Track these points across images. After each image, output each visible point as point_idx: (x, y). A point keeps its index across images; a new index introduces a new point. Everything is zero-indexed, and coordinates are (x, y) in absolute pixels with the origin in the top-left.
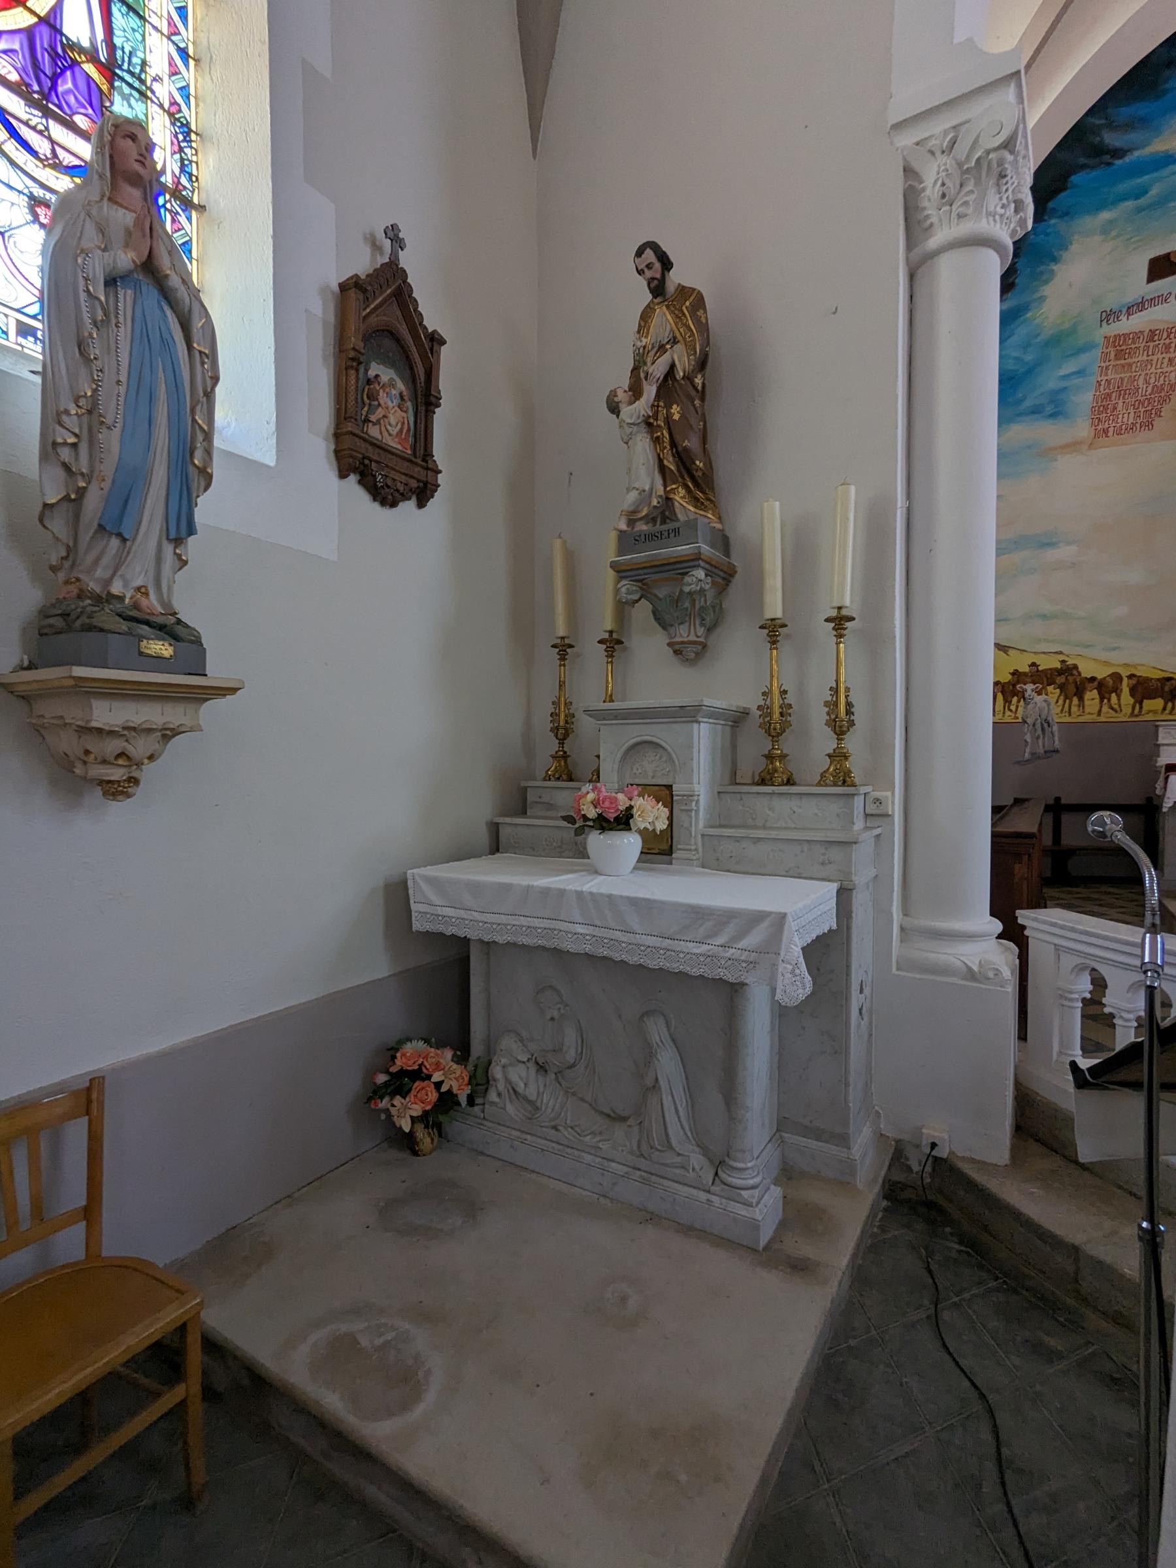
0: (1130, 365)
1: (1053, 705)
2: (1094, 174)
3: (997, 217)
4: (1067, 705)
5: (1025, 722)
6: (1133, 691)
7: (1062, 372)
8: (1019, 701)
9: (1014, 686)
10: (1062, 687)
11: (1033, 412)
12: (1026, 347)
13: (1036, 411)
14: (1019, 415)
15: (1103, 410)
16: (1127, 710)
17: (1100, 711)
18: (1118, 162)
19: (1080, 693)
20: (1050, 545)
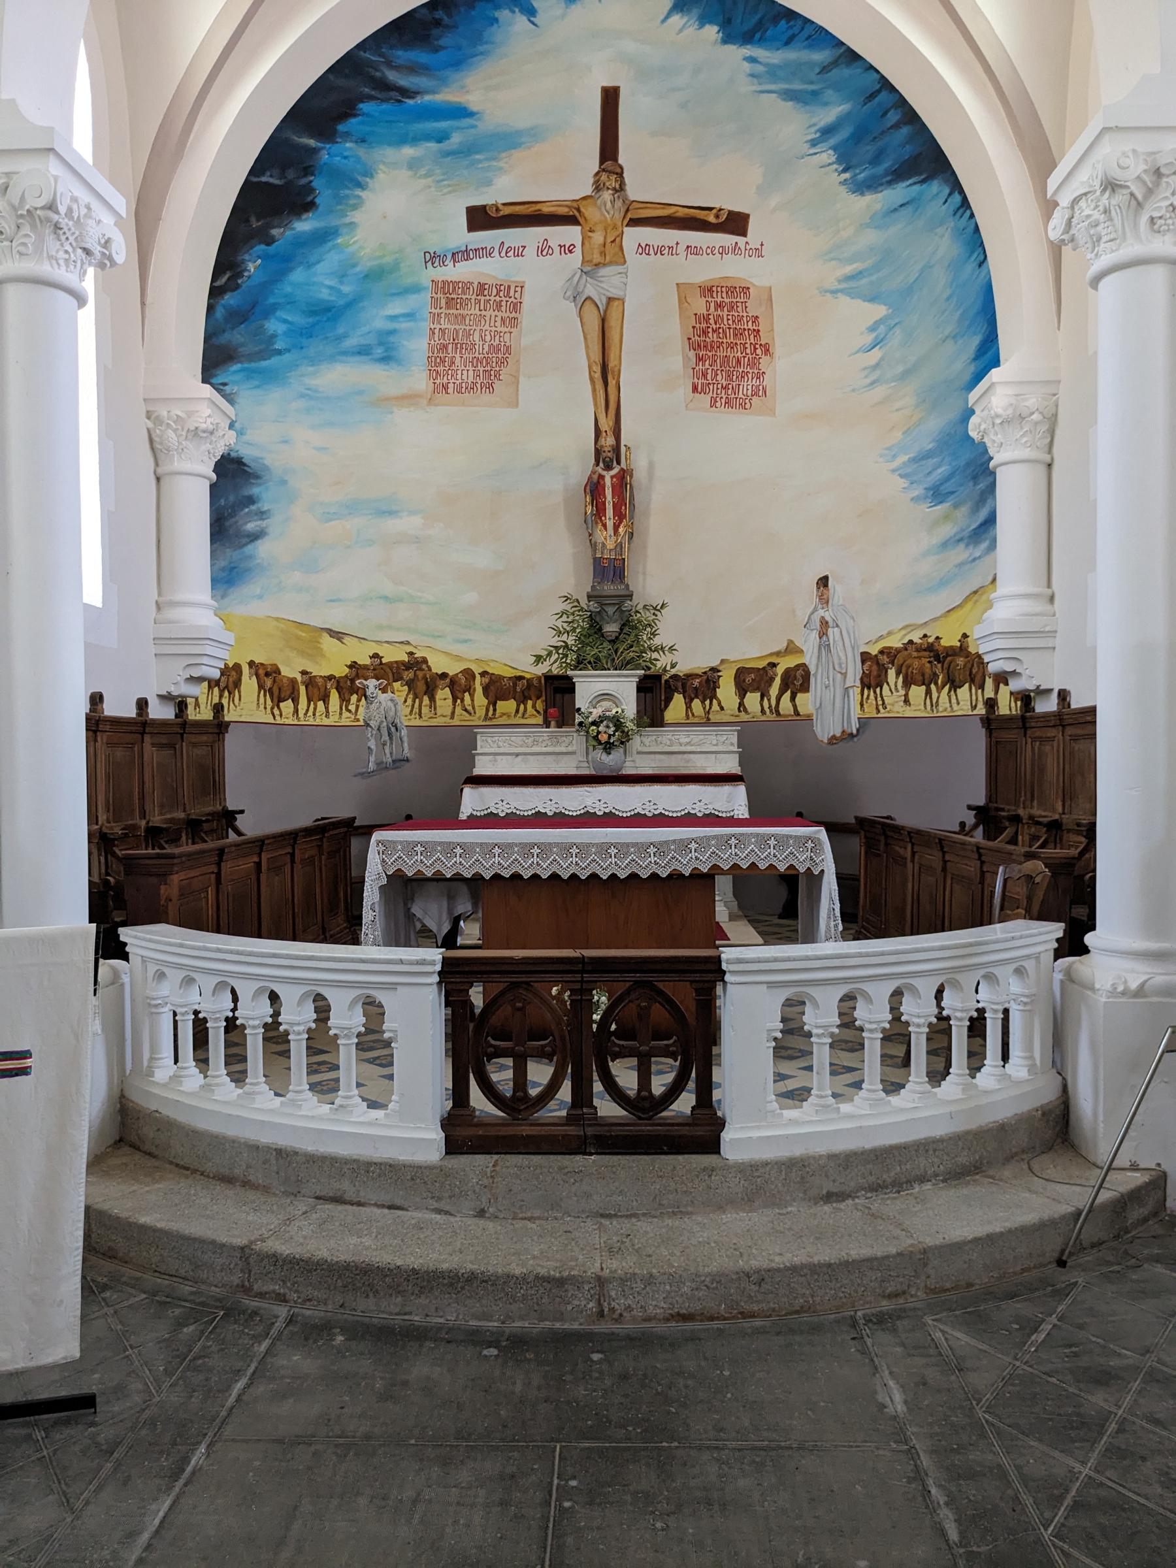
0: (464, 317)
1: (400, 706)
2: (384, 106)
3: (62, 262)
4: (417, 705)
5: (367, 725)
6: (486, 690)
7: (390, 311)
8: (359, 700)
9: (353, 681)
10: (410, 684)
11: (359, 353)
12: (342, 276)
13: (363, 351)
14: (345, 353)
15: (439, 361)
16: (481, 712)
17: (453, 713)
18: (411, 102)
19: (430, 691)
20: (391, 513)
